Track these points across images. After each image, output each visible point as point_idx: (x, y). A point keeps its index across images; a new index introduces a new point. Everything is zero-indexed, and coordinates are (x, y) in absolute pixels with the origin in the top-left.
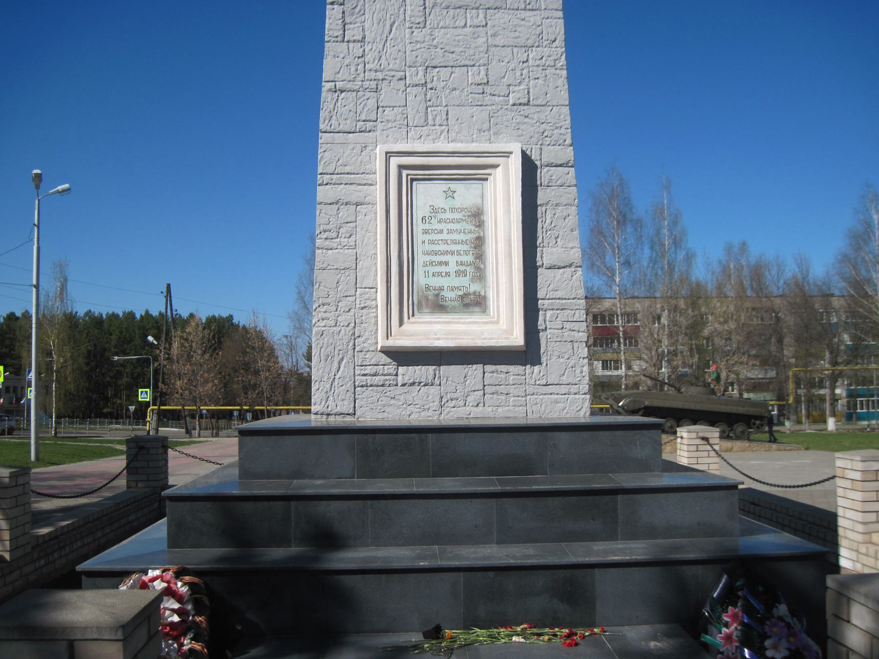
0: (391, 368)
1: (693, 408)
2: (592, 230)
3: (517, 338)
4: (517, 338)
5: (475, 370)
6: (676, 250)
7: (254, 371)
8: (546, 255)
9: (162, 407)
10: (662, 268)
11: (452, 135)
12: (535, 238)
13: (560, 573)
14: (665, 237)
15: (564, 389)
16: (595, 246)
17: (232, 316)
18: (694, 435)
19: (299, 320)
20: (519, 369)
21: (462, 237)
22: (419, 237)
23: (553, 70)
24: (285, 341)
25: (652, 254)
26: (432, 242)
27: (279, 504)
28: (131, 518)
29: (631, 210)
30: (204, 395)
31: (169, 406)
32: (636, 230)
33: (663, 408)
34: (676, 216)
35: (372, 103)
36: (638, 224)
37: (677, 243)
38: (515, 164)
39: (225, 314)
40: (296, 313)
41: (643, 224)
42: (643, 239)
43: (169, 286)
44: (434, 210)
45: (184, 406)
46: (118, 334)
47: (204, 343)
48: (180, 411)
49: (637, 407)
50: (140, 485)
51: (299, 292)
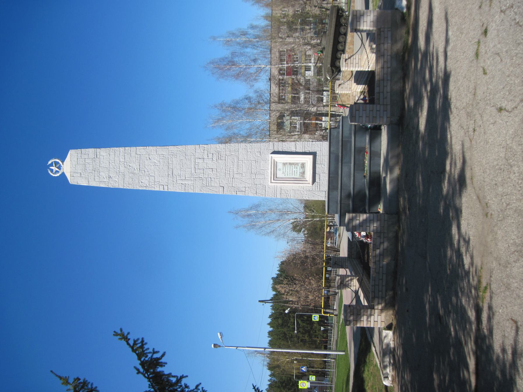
0: (316, 183)
1: (332, 44)
2: (237, 79)
3: (311, 157)
4: (311, 157)
5: (317, 166)
6: (248, 34)
7: (306, 258)
8: (293, 150)
9: (323, 307)
10: (258, 42)
11: (267, 169)
12: (290, 152)
13: (356, 153)
14: (241, 40)
15: (322, 147)
16: (245, 78)
17: (272, 278)
18: (338, 89)
19: (279, 236)
20: (317, 156)
21: (289, 167)
22: (289, 176)
23: (253, 146)
24: (290, 243)
25: (250, 47)
26: (290, 174)
27: (342, 205)
28: (355, 263)
29: (226, 58)
30: (317, 284)
31: (322, 303)
32: (237, 56)
33: (332, 58)
34: (230, 33)
35: (259, 186)
36: (233, 54)
37: (244, 34)
38: (274, 156)
39: (271, 282)
40: (276, 237)
41: (234, 51)
42: (242, 52)
43: (260, 301)
44: (283, 173)
45: (322, 296)
46: (280, 340)
47: (290, 284)
48: (325, 298)
49: (331, 71)
50: (347, 264)
51: (265, 235)
